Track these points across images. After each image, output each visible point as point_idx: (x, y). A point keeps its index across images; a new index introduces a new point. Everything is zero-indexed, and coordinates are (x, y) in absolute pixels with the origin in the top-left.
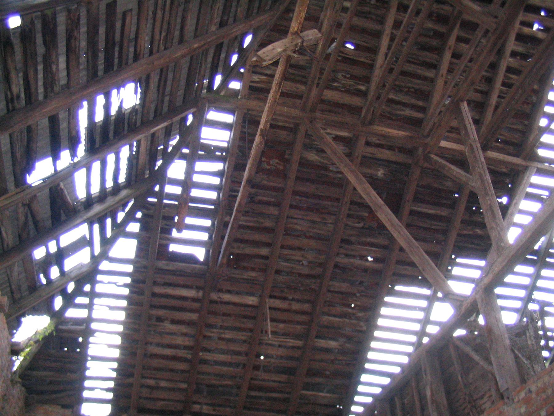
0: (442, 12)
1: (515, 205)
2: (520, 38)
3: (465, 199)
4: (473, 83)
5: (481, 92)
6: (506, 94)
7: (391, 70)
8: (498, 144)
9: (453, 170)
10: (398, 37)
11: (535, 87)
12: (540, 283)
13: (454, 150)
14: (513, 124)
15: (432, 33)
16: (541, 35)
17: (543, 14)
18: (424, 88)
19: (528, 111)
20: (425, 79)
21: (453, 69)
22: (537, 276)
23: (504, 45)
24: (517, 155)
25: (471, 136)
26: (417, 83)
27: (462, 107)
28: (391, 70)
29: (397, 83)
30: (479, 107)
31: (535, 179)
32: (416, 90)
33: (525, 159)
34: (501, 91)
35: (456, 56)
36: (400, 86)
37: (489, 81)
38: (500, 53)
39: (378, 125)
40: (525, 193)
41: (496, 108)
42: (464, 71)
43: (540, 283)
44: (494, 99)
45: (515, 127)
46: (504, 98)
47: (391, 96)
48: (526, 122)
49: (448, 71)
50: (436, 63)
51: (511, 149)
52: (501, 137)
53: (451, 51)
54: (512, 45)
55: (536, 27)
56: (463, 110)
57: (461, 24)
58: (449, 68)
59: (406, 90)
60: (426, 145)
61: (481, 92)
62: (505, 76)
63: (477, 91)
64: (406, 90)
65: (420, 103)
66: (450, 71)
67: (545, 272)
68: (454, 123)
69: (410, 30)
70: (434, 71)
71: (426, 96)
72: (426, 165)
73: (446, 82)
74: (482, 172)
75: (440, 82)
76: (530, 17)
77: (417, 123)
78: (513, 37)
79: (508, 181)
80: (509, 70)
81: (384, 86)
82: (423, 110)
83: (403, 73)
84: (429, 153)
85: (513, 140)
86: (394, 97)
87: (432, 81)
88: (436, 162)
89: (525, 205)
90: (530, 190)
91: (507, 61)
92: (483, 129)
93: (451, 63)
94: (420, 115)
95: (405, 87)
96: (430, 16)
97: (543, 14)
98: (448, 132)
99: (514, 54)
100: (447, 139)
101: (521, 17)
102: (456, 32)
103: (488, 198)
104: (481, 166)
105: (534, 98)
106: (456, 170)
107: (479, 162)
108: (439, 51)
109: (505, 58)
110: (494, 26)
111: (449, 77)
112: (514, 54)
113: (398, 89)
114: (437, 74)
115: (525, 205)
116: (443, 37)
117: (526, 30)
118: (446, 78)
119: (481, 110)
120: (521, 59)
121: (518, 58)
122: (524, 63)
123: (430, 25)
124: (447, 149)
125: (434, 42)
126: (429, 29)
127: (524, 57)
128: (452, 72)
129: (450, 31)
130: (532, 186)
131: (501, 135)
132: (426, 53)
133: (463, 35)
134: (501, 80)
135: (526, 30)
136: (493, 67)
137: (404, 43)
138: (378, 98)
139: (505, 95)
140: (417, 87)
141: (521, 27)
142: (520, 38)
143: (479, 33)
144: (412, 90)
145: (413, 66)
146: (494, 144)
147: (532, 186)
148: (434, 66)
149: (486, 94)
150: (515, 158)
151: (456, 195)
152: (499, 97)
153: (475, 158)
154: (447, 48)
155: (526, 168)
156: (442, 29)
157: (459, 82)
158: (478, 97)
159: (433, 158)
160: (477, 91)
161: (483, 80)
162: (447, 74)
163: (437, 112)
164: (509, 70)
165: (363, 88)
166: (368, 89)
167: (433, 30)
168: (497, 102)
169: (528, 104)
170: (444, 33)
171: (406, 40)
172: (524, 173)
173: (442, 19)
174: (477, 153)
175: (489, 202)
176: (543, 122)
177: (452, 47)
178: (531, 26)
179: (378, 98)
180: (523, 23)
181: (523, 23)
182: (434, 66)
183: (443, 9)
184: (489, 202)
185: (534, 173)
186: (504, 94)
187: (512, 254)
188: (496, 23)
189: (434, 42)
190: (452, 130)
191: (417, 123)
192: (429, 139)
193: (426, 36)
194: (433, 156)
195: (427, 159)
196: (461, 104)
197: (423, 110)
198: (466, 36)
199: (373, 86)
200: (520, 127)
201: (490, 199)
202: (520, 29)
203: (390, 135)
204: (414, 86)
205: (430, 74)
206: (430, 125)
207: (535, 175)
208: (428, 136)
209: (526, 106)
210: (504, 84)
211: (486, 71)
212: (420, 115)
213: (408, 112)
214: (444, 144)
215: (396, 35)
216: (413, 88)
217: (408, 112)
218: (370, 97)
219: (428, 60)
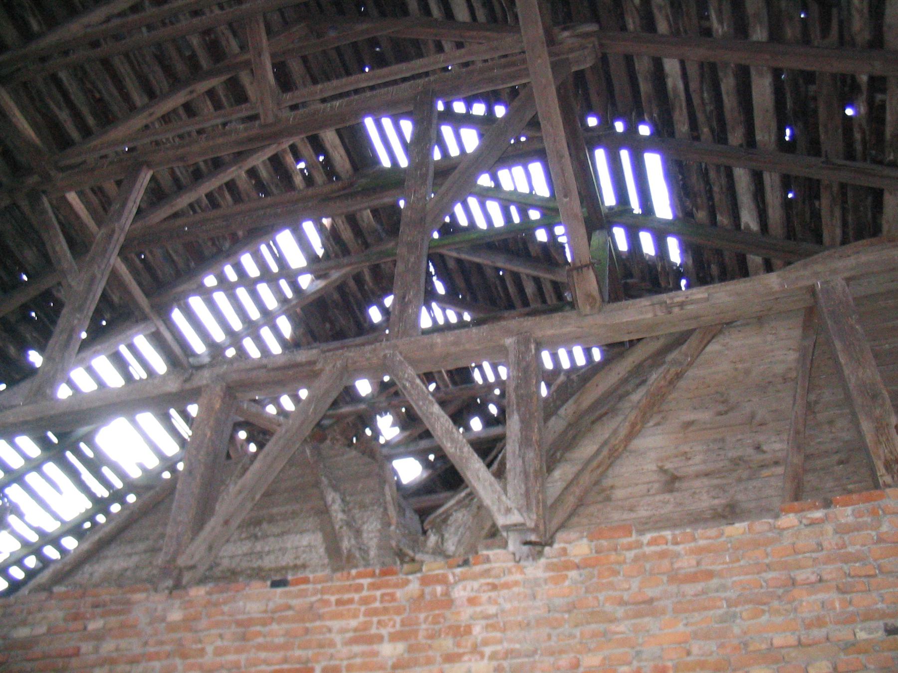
0: (224, 43)
1: (94, 352)
2: (276, 162)
3: (33, 292)
4: (182, 159)
5: (176, 180)
6: (203, 211)
7: (95, 44)
8: (137, 261)
9: (60, 242)
10: (143, 14)
11: (240, 233)
12: (32, 478)
13: (78, 217)
14: (176, 252)
15: (188, 53)
16: (298, 180)
17: (321, 158)
18: (115, 108)
19: (207, 253)
20: (127, 97)
21: (170, 121)
22: (35, 466)
23: (252, 152)
24: (147, 294)
25: (123, 220)
26: (109, 91)
27: (143, 174)
28: (95, 44)
29: (87, 67)
30: (157, 195)
31: (141, 342)
32: (101, 100)
33: (152, 307)
34: (198, 201)
35: (189, 109)
36: (85, 72)
37: (197, 176)
38: (240, 156)
39: (9, 93)
40: (114, 350)
41: (175, 215)
42: (181, 137)
43: (32, 478)
44: (183, 202)
45: (175, 258)
46: (195, 212)
47: (63, 75)
48: (192, 264)
49: (163, 117)
50: (158, 92)
51: (146, 278)
52: (147, 253)
53: (188, 98)
54: (259, 160)
55: (302, 165)
56: (140, 179)
57: (232, 77)
58: (168, 114)
59: (89, 86)
60: (46, 178)
61: (176, 180)
62: (220, 188)
63: (172, 172)
64: (89, 86)
65: (91, 121)
66: (166, 119)
67: (50, 468)
68: (110, 187)
69: (167, 21)
70: (146, 100)
71: (107, 119)
72: (24, 204)
73: (147, 127)
74: (99, 276)
75: (138, 122)
76: (306, 150)
77: (64, 142)
78: (269, 152)
79: (108, 316)
80: (231, 186)
81: (66, 53)
82: (87, 133)
83: (106, 63)
84: (44, 192)
85: (159, 272)
86: (64, 79)
87: (133, 109)
88: (43, 212)
89: (102, 363)
90: (123, 349)
91: (237, 173)
92: (139, 224)
93: (175, 111)
94: (75, 135)
95: (93, 83)
96: (207, 32)
97: (321, 158)
98: (92, 190)
99: (252, 173)
100: (81, 194)
101: (296, 140)
102: (215, 82)
103: (78, 316)
104: (103, 267)
105: (227, 245)
106: (61, 245)
107: (105, 261)
108: (176, 83)
109: (240, 167)
110: (271, 119)
111: (157, 126)
112: (252, 173)
113: (80, 73)
114: (144, 108)
115: (102, 363)
116: (196, 71)
117: (289, 159)
118: (153, 123)
119: (155, 200)
120: (255, 185)
121: (253, 182)
122: (253, 194)
123: (195, 41)
124: (70, 206)
125: (180, 67)
126: (189, 46)
127: (261, 186)
128: (166, 123)
129: (211, 74)
130: (132, 347)
131: (151, 252)
132: (157, 68)
133: (221, 93)
134: (212, 188)
135: (289, 159)
136: (217, 164)
137: (144, 29)
138: (43, 59)
139: (199, 211)
140: (106, 97)
141: (288, 150)
142: (276, 162)
143: (244, 111)
144: (97, 95)
145: (127, 66)
146: (133, 255)
147: (132, 347)
148: (151, 94)
149: (180, 187)
150: (143, 296)
151: (25, 278)
152: (191, 206)
153: (105, 250)
154: (189, 89)
155: (145, 318)
156: (205, 62)
157: (164, 143)
158: (166, 181)
159: (43, 203)
160: (172, 172)
161: (191, 169)
162: (158, 119)
163: (103, 152)
164: (231, 186)
165: (35, 26)
166: (40, 35)
167: (193, 51)
168: (182, 210)
169: (214, 244)
170: (201, 67)
171: (150, 28)
172: (137, 322)
173: (215, 50)
174: (111, 246)
175: (76, 322)
176: (210, 281)
177: (194, 95)
178: (298, 161)
179: (43, 59)
180: (294, 149)
181: (294, 149)
182: (151, 94)
183: (227, 40)
184: (76, 322)
185: (148, 332)
186: (200, 207)
187: (52, 412)
188: (276, 116)
189: (180, 67)
190: (99, 191)
191: (64, 142)
192: (61, 175)
193: (179, 50)
194: (45, 200)
195: (34, 196)
196: (145, 168)
197: (87, 133)
198: (223, 99)
199: (52, 38)
200: (181, 264)
201: (79, 320)
202: (284, 151)
203: (14, 120)
204: (104, 92)
205: (138, 98)
206: (79, 160)
207: (146, 336)
208: (62, 170)
209: (210, 244)
210: (209, 196)
211: (205, 161)
212: (75, 135)
213: (64, 116)
214: (72, 197)
215: (144, 9)
216: (100, 92)
217: (64, 116)
218: (33, 46)
219: (151, 77)
